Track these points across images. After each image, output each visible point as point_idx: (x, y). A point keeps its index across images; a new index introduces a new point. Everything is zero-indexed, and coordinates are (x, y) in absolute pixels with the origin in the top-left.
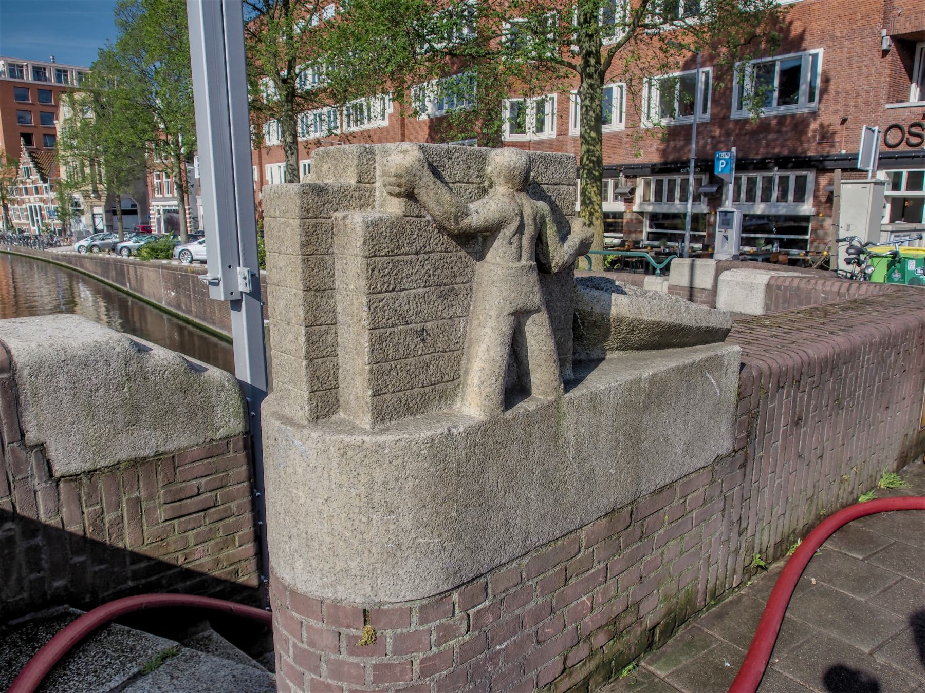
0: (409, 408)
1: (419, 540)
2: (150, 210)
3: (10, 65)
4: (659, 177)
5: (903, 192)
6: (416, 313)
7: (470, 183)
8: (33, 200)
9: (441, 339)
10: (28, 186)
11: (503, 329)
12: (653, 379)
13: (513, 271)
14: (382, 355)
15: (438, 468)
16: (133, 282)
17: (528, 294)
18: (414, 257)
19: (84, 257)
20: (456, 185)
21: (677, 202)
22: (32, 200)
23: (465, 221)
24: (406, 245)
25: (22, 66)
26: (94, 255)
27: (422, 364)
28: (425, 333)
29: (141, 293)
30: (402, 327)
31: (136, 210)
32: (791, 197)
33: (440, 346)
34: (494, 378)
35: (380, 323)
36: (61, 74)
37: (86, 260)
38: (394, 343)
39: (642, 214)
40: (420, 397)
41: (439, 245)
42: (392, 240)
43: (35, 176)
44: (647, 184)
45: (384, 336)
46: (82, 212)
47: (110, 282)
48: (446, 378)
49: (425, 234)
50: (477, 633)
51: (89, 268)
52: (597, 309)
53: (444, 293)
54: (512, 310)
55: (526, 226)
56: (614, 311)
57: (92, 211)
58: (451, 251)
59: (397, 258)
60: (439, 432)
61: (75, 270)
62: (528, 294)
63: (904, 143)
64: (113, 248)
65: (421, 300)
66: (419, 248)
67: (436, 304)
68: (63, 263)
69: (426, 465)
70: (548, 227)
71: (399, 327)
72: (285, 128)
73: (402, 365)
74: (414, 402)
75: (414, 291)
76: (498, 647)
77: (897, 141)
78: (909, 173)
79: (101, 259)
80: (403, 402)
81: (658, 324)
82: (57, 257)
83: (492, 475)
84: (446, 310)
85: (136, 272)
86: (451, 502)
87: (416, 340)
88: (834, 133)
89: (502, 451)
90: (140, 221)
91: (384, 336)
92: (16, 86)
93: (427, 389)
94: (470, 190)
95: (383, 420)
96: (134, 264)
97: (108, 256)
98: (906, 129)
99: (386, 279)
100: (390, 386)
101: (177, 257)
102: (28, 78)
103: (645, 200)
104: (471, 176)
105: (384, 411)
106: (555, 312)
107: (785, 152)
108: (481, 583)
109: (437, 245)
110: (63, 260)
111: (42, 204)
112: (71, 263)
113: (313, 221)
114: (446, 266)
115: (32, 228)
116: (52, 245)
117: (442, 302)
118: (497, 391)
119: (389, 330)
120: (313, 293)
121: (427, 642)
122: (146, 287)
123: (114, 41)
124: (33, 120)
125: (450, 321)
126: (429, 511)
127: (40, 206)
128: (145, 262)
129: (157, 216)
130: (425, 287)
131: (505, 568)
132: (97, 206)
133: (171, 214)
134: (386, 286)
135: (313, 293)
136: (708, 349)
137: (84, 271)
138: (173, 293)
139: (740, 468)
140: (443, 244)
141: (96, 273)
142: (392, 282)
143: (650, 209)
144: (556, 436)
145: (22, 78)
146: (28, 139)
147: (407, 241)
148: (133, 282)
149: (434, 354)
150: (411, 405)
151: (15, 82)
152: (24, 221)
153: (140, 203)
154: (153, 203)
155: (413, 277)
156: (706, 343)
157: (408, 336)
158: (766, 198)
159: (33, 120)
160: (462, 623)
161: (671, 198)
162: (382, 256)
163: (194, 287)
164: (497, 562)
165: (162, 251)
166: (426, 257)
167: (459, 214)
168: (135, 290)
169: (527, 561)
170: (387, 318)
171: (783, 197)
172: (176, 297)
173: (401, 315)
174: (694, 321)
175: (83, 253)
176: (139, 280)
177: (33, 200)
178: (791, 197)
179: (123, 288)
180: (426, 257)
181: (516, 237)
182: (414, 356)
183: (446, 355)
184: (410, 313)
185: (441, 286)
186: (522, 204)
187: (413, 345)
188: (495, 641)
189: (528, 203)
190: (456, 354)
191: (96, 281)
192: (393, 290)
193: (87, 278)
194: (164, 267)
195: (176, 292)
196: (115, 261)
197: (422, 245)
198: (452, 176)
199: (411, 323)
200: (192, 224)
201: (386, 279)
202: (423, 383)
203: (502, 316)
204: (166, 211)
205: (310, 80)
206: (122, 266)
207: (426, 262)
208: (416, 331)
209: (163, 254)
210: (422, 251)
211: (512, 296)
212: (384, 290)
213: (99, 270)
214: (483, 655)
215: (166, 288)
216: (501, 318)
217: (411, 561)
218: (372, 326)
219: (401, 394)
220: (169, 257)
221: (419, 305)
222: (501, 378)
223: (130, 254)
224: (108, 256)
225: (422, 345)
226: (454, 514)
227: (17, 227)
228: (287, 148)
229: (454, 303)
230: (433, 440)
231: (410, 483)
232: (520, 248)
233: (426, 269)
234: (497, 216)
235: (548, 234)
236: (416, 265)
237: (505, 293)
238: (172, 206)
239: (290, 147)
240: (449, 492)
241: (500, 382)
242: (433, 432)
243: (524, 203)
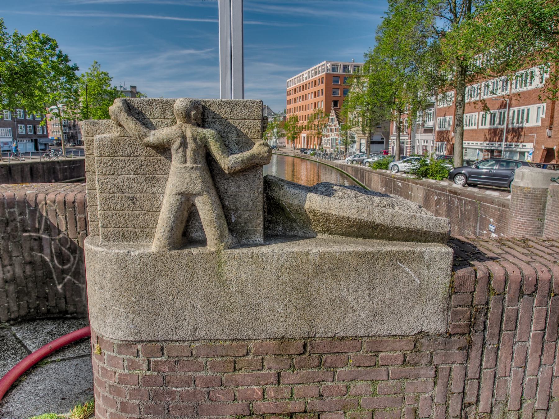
0: (125, 238)
1: (114, 307)
2: (389, 142)
3: (333, 65)
6: (129, 188)
7: (166, 119)
11: (171, 202)
13: (179, 169)
14: (107, 207)
16: (367, 181)
17: (189, 184)
18: (127, 158)
19: (348, 166)
20: (155, 120)
23: (146, 139)
24: (120, 151)
26: (353, 165)
27: (133, 216)
28: (135, 200)
29: (370, 188)
31: (383, 142)
33: (146, 207)
34: (163, 230)
35: (105, 191)
36: (345, 68)
37: (349, 168)
38: (114, 202)
40: (132, 233)
42: (111, 148)
43: (336, 122)
45: (107, 197)
46: (355, 142)
47: (357, 180)
49: (133, 146)
50: (155, 373)
51: (350, 172)
55: (189, 143)
56: (307, 205)
57: (360, 141)
59: (115, 158)
60: (122, 252)
61: (344, 173)
62: (189, 184)
64: (362, 162)
65: (132, 181)
66: (129, 154)
67: (143, 185)
68: (339, 169)
69: (115, 268)
70: (211, 145)
71: (118, 194)
72: (458, 91)
73: (120, 214)
74: (128, 235)
75: (127, 176)
76: (174, 389)
79: (355, 168)
80: (121, 234)
83: (161, 285)
84: (150, 188)
85: (369, 176)
86: (131, 292)
89: (169, 272)
90: (384, 148)
91: (107, 197)
92: (334, 76)
93: (137, 230)
94: (166, 123)
95: (108, 241)
96: (369, 171)
97: (359, 166)
99: (108, 168)
100: (112, 224)
102: (340, 72)
105: (109, 236)
108: (158, 346)
109: (143, 152)
111: (337, 137)
112: (342, 169)
113: (91, 138)
114: (149, 164)
115: (331, 150)
116: (336, 159)
117: (147, 183)
118: (164, 237)
119: (111, 195)
122: (372, 185)
123: (373, 48)
125: (152, 195)
126: (118, 293)
127: (336, 138)
128: (374, 171)
129: (392, 145)
130: (134, 174)
131: (178, 343)
132: (363, 139)
134: (108, 172)
135: (91, 173)
137: (347, 173)
138: (384, 189)
139: (461, 349)
140: (146, 152)
141: (352, 175)
142: (112, 170)
145: (337, 71)
146: (336, 103)
147: (122, 149)
148: (367, 181)
149: (141, 211)
150: (126, 236)
152: (328, 146)
154: (392, 138)
155: (126, 169)
157: (123, 200)
159: (339, 93)
160: (144, 363)
162: (106, 156)
163: (394, 186)
166: (135, 158)
167: (141, 135)
168: (367, 186)
170: (109, 188)
172: (385, 191)
173: (118, 188)
174: (389, 221)
175: (349, 164)
176: (370, 180)
177: (333, 135)
179: (362, 184)
180: (135, 158)
181: (181, 149)
182: (128, 210)
183: (150, 213)
184: (125, 187)
186: (185, 130)
187: (127, 205)
191: (352, 180)
192: (113, 174)
194: (382, 174)
195: (386, 189)
196: (361, 169)
197: (131, 152)
198: (152, 115)
199: (125, 193)
200: (411, 150)
201: (108, 168)
202: (134, 226)
203: (172, 195)
205: (479, 61)
207: (135, 161)
208: (129, 197)
209: (385, 166)
210: (132, 155)
211: (178, 184)
212: (107, 174)
213: (354, 174)
215: (381, 186)
216: (171, 196)
217: (111, 317)
218: (100, 191)
219: (120, 229)
220: (387, 168)
223: (370, 166)
224: (359, 166)
225: (133, 205)
226: (133, 299)
227: (324, 149)
228: (458, 104)
229: (156, 185)
230: (118, 255)
231: (109, 275)
232: (185, 155)
233: (135, 165)
234: (165, 137)
235: (212, 149)
236: (128, 162)
237: (174, 182)
239: (460, 103)
240: (129, 286)
241: (166, 232)
243: (187, 130)
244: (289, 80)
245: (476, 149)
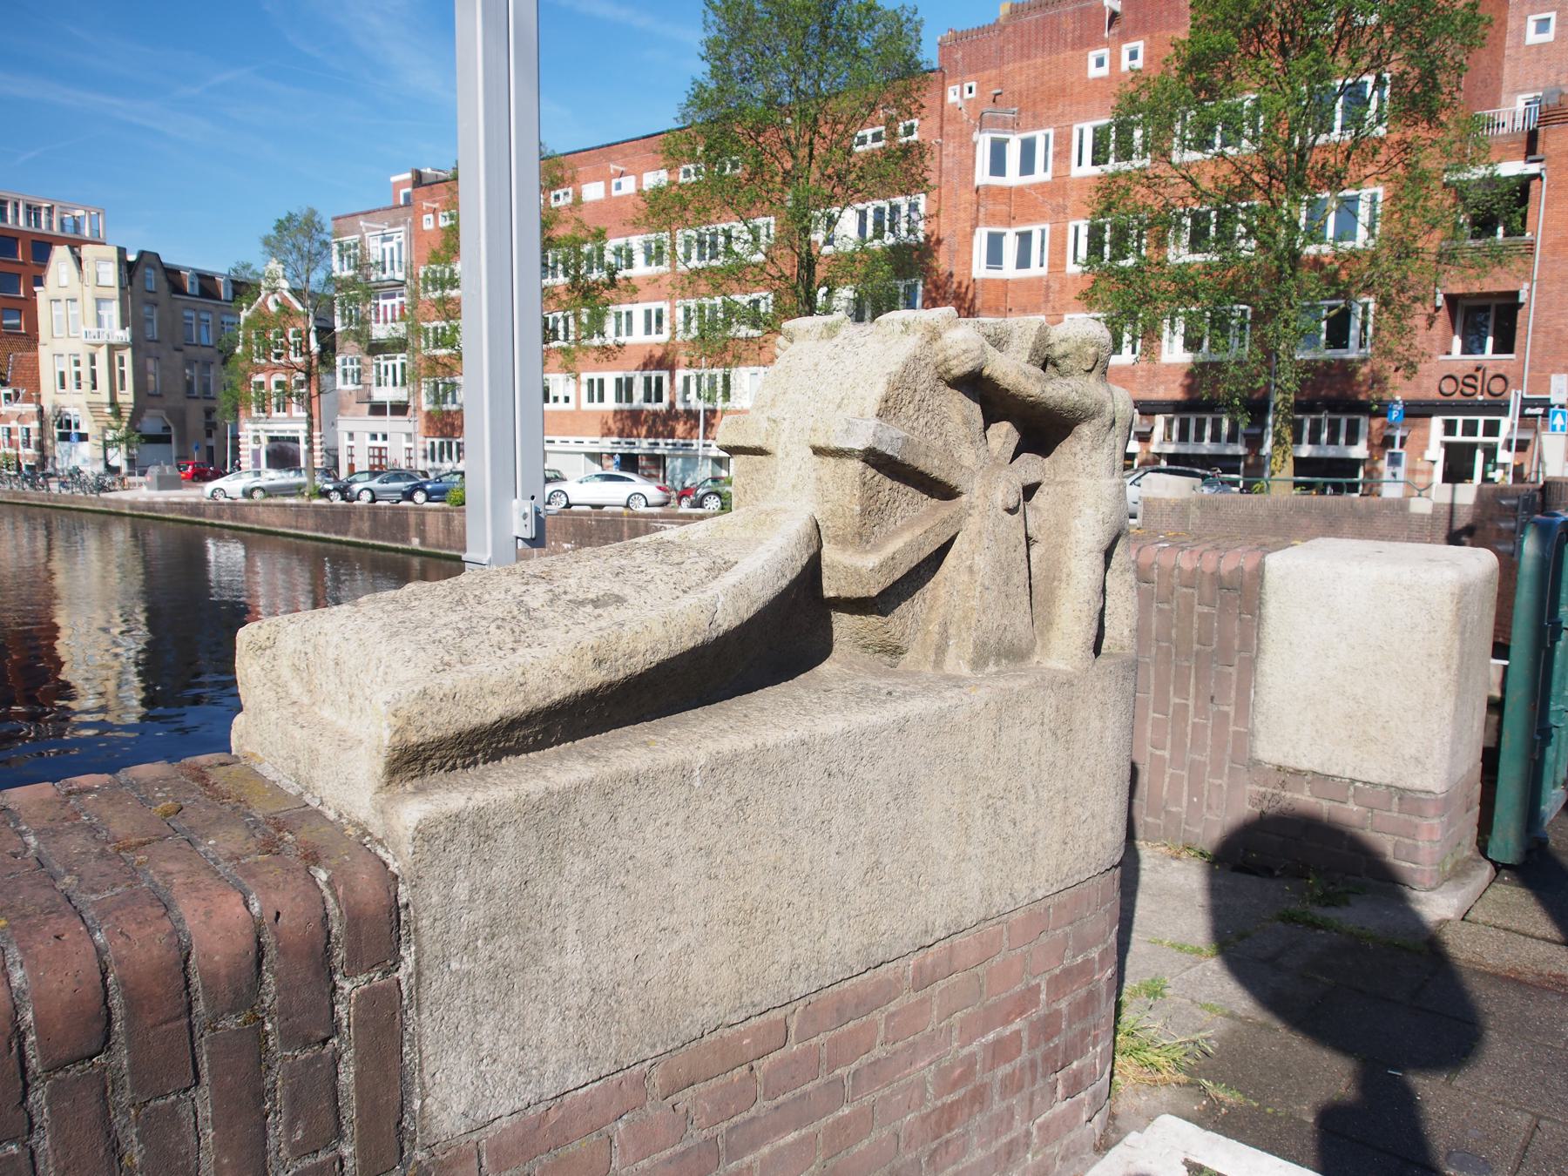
4: (1185, 416)
5: (1459, 438)
21: (1207, 441)
25: (40, 208)
31: (170, 437)
32: (1342, 440)
39: (1159, 455)
44: (1169, 423)
51: (274, 522)
63: (1458, 393)
77: (1452, 390)
78: (1486, 421)
88: (1386, 378)
98: (1460, 380)
102: (17, 223)
103: (1168, 436)
107: (1333, 394)
110: (172, 511)
133: (283, 444)
143: (1170, 449)
158: (1314, 440)
161: (1199, 438)
171: (1333, 440)
178: (1342, 440)
193: (249, 534)
204: (272, 439)
238: (285, 431)
245: (580, 453)
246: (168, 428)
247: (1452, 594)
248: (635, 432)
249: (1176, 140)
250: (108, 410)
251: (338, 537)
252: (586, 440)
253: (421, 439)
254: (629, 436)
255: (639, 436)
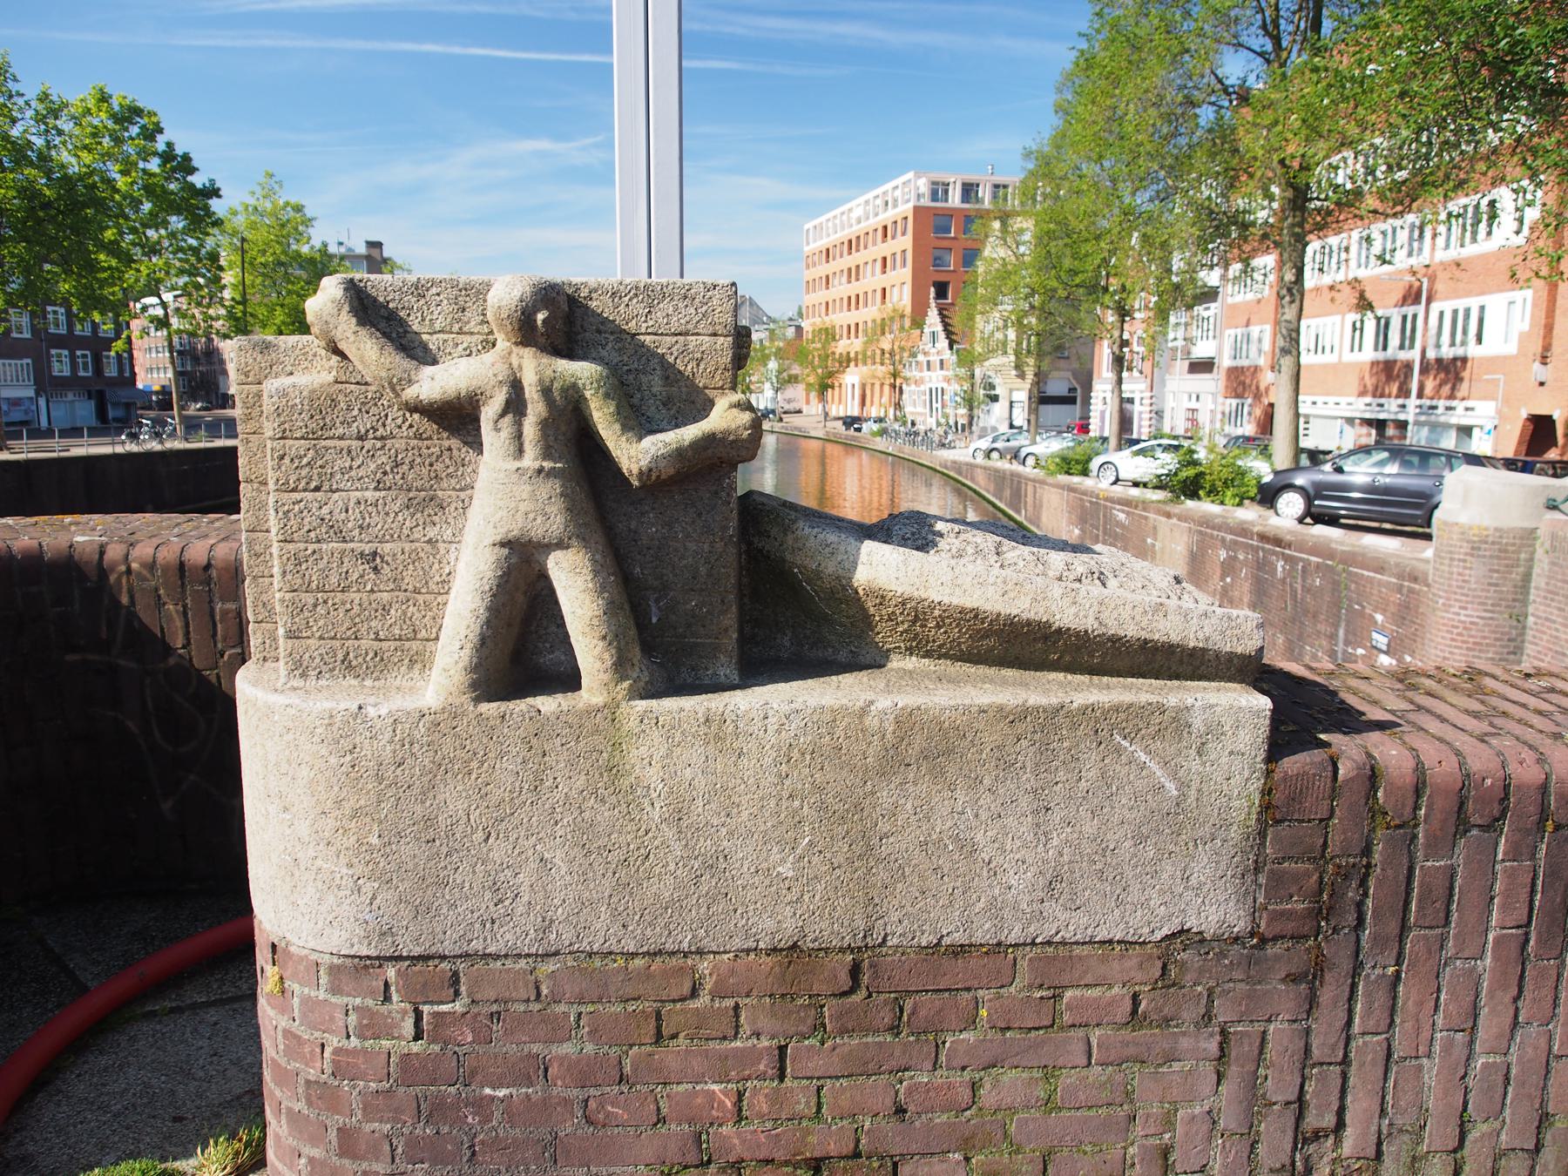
1: (319, 862)
3: (934, 183)
6: (361, 527)
7: (466, 333)
8: (935, 379)
9: (410, 572)
10: (931, 358)
11: (481, 568)
12: (907, 721)
14: (299, 581)
15: (342, 760)
18: (355, 444)
20: (435, 336)
22: (934, 379)
24: (338, 425)
27: (374, 605)
28: (378, 560)
29: (1038, 527)
30: (335, 545)
31: (1075, 398)
33: (409, 581)
40: (371, 655)
41: (404, 428)
42: (312, 417)
43: (943, 343)
45: (302, 553)
47: (1002, 506)
48: (423, 634)
49: (374, 410)
51: (981, 484)
52: (830, 567)
53: (415, 502)
54: (498, 538)
55: (529, 402)
58: (430, 438)
59: (324, 443)
60: (342, 706)
61: (964, 485)
62: (531, 516)
65: (370, 508)
66: (363, 431)
67: (400, 518)
69: (324, 752)
71: (331, 545)
72: (1286, 255)
73: (337, 600)
76: (488, 1091)
81: (976, 614)
82: (957, 466)
84: (420, 528)
86: (368, 820)
87: (361, 568)
89: (474, 764)
90: (1078, 415)
91: (302, 553)
92: (937, 213)
93: (385, 645)
94: (465, 345)
95: (304, 675)
96: (1034, 481)
99: (304, 472)
100: (315, 629)
101: (1095, 473)
104: (469, 322)
105: (305, 664)
106: (682, 557)
108: (443, 971)
109: (400, 427)
111: (945, 385)
112: (960, 473)
114: (418, 460)
118: (461, 665)
119: (311, 547)
120: (256, 486)
121: (341, 1024)
122: (1044, 519)
124: (952, 262)
125: (428, 547)
128: (1050, 480)
130: (376, 489)
131: (499, 963)
135: (256, 486)
136: (1130, 688)
140: (411, 426)
141: (988, 491)
144: (613, 770)
145: (947, 201)
147: (341, 419)
148: (1030, 508)
149: (397, 593)
150: (354, 663)
151: (936, 208)
152: (920, 409)
153: (1082, 387)
155: (353, 473)
156: (1178, 678)
159: (952, 262)
160: (403, 1020)
162: (296, 439)
163: (1105, 523)
164: (477, 945)
165: (1077, 462)
166: (379, 444)
167: (395, 380)
168: (1031, 522)
169: (552, 968)
170: (306, 529)
173: (332, 527)
176: (1038, 507)
177: (935, 379)
182: (359, 591)
183: (421, 598)
184: (350, 525)
185: (409, 490)
187: (356, 575)
188: (479, 1078)
189: (533, 366)
190: (439, 599)
192: (317, 489)
195: (1081, 530)
196: (1013, 474)
197: (369, 426)
198: (427, 322)
199: (352, 541)
200: (1153, 422)
202: (377, 634)
206: (1019, 482)
208: (362, 554)
210: (371, 435)
212: (300, 487)
213: (992, 488)
214: (452, 1089)
218: (281, 537)
219: (337, 644)
220: (1085, 472)
221: (367, 516)
222: (469, 645)
223: (1037, 465)
225: (372, 576)
226: (374, 840)
228: (1284, 292)
229: (436, 519)
239: (1289, 290)
240: (362, 802)
242: (334, 704)
244: (809, 225)
246: (1075, 389)
247: (604, 638)
248: (1387, 391)
249: (698, 1088)
250: (1014, 372)
251: (956, 476)
252: (1343, 400)
253: (1221, 399)
254: (1382, 396)
255: (1389, 396)
